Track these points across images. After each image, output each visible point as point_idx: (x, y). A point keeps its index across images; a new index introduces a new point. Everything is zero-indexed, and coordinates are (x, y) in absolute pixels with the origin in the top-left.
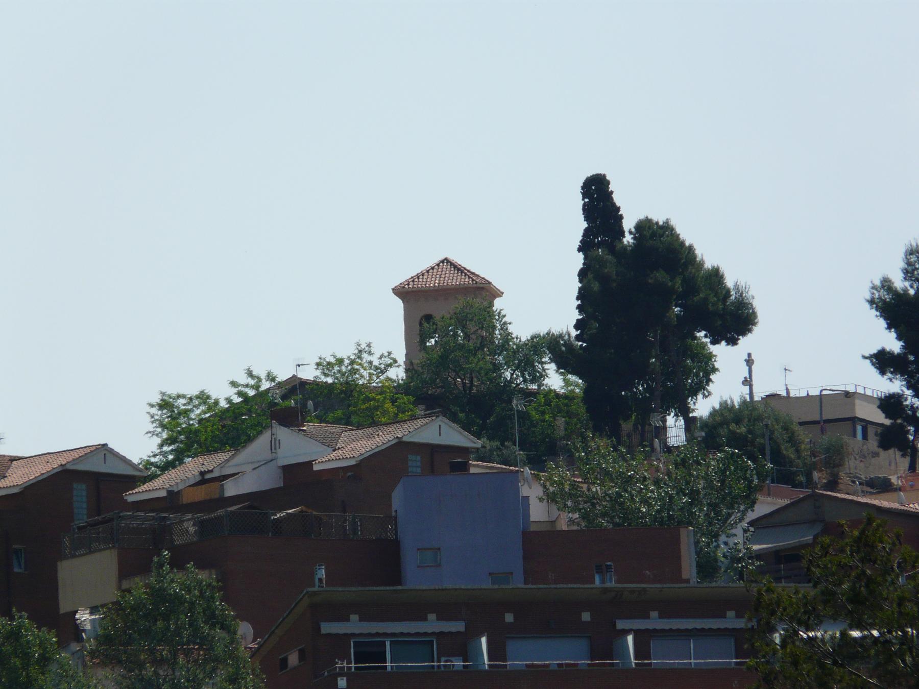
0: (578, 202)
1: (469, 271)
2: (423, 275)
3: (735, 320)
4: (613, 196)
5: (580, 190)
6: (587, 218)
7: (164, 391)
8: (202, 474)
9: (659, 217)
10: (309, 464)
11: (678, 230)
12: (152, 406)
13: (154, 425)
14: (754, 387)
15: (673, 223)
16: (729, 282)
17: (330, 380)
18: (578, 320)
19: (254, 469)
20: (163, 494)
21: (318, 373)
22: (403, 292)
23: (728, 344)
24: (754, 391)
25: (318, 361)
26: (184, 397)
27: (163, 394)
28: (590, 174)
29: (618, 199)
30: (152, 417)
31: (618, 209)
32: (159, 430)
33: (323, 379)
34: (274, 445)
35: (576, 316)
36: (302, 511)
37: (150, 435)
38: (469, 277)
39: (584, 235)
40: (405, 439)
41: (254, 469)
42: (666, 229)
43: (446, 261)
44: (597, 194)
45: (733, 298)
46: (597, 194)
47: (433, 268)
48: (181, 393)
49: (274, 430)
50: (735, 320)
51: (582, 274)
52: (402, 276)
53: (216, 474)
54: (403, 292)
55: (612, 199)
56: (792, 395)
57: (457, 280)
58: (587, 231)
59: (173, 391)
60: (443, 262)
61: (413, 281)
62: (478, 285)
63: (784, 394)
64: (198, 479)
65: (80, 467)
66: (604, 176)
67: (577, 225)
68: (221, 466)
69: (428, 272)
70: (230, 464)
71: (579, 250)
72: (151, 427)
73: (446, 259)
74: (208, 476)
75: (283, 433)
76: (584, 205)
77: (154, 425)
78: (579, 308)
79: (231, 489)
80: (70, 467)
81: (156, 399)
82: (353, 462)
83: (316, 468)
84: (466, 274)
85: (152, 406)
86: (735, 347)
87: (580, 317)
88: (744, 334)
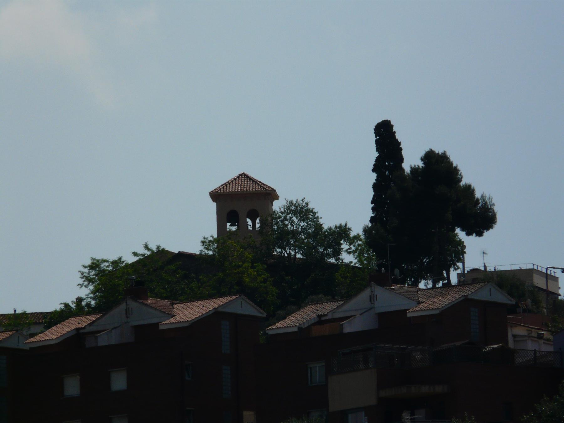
0: (372, 138)
1: (260, 182)
2: (229, 184)
3: (481, 219)
4: (396, 135)
5: (373, 131)
6: (378, 150)
7: (94, 257)
8: (319, 316)
9: (439, 150)
10: (404, 312)
11: (452, 159)
12: (85, 267)
13: (83, 280)
14: (465, 263)
15: (448, 154)
16: (478, 195)
17: (211, 253)
18: (372, 217)
19: (361, 314)
20: (296, 329)
21: (202, 248)
22: (215, 196)
23: (476, 236)
24: (465, 266)
25: (203, 240)
26: (107, 261)
27: (93, 259)
28: (380, 121)
29: (398, 136)
30: (82, 274)
31: (399, 144)
32: (86, 283)
33: (206, 252)
34: (372, 298)
35: (370, 214)
36: (502, 347)
37: (80, 286)
38: (258, 185)
39: (376, 161)
40: (469, 297)
41: (361, 314)
42: (444, 158)
43: (244, 175)
44: (385, 134)
45: (480, 205)
46: (385, 134)
47: (235, 179)
48: (105, 258)
49: (373, 288)
50: (481, 219)
51: (375, 187)
52: (216, 184)
53: (329, 317)
54: (215, 196)
55: (395, 136)
56: (488, 270)
57: (252, 188)
58: (378, 159)
59: (99, 257)
60: (241, 175)
61: (223, 188)
62: (268, 192)
63: (483, 269)
64: (317, 320)
65: (227, 310)
66: (390, 121)
67: (372, 154)
68: (333, 311)
69: (232, 182)
70: (340, 310)
71: (374, 170)
72: (81, 281)
73: (243, 173)
74: (324, 318)
75: (379, 291)
76: (376, 141)
77: (83, 280)
78: (373, 209)
79: (348, 328)
80: (220, 309)
81: (89, 262)
82: (437, 312)
83: (409, 315)
84: (258, 185)
85: (85, 267)
86: (481, 237)
87: (373, 215)
88: (488, 229)
